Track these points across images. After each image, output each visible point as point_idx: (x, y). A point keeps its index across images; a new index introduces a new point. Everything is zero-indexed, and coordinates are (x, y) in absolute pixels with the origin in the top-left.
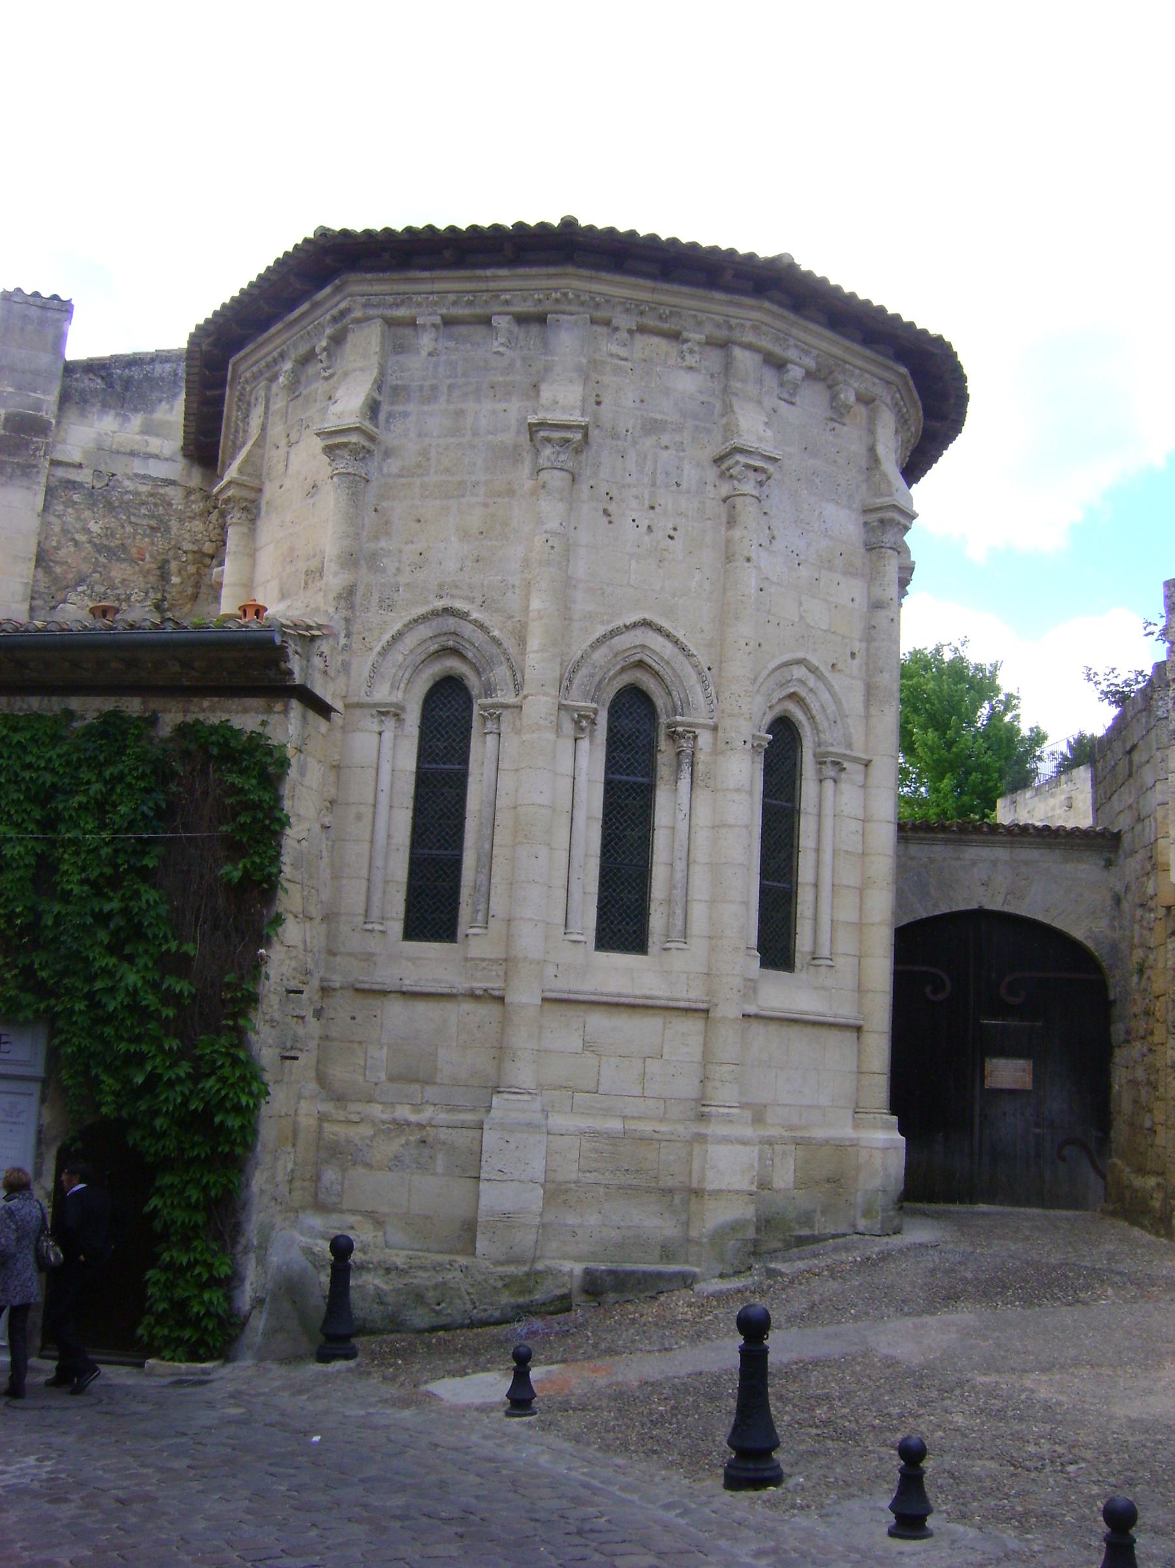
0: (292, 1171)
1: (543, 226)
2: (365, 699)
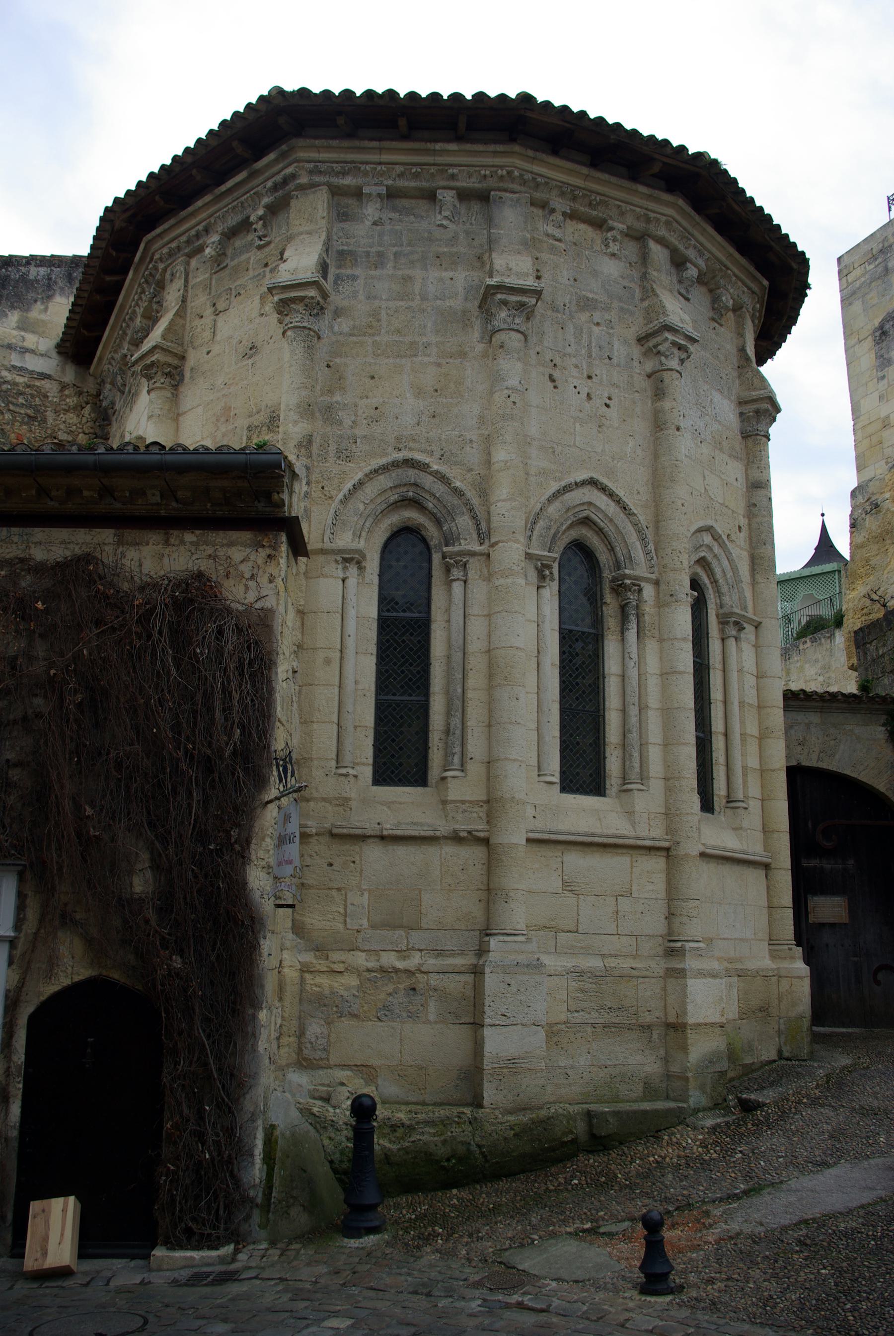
0: (281, 1026)
1: (503, 97)
2: (328, 545)
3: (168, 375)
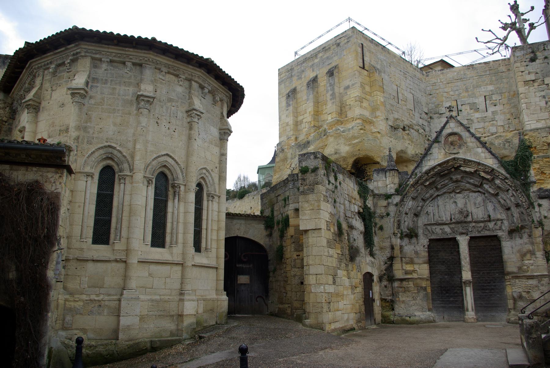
1: (146, 38)
2: (82, 171)
3: (35, 108)
